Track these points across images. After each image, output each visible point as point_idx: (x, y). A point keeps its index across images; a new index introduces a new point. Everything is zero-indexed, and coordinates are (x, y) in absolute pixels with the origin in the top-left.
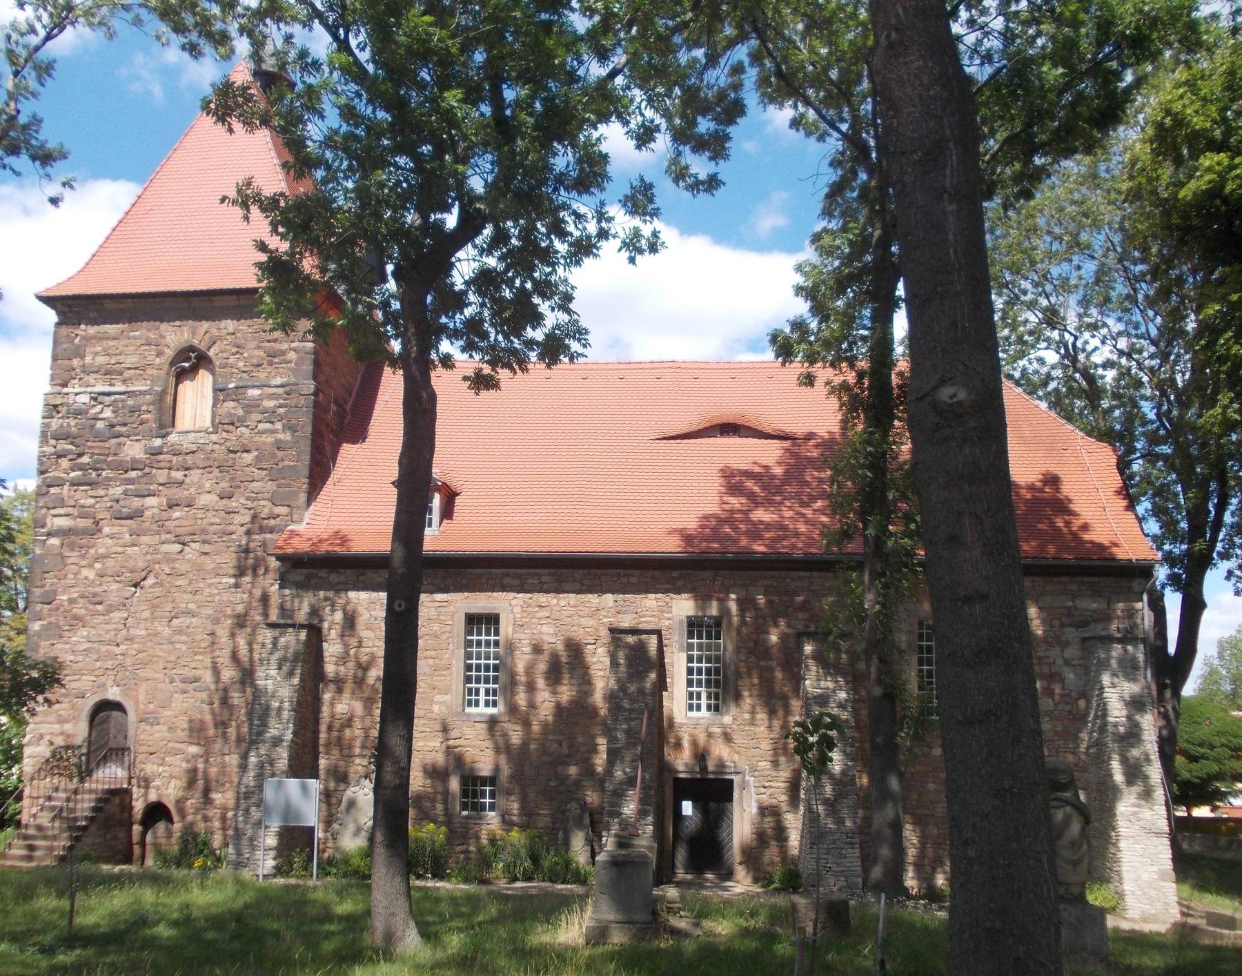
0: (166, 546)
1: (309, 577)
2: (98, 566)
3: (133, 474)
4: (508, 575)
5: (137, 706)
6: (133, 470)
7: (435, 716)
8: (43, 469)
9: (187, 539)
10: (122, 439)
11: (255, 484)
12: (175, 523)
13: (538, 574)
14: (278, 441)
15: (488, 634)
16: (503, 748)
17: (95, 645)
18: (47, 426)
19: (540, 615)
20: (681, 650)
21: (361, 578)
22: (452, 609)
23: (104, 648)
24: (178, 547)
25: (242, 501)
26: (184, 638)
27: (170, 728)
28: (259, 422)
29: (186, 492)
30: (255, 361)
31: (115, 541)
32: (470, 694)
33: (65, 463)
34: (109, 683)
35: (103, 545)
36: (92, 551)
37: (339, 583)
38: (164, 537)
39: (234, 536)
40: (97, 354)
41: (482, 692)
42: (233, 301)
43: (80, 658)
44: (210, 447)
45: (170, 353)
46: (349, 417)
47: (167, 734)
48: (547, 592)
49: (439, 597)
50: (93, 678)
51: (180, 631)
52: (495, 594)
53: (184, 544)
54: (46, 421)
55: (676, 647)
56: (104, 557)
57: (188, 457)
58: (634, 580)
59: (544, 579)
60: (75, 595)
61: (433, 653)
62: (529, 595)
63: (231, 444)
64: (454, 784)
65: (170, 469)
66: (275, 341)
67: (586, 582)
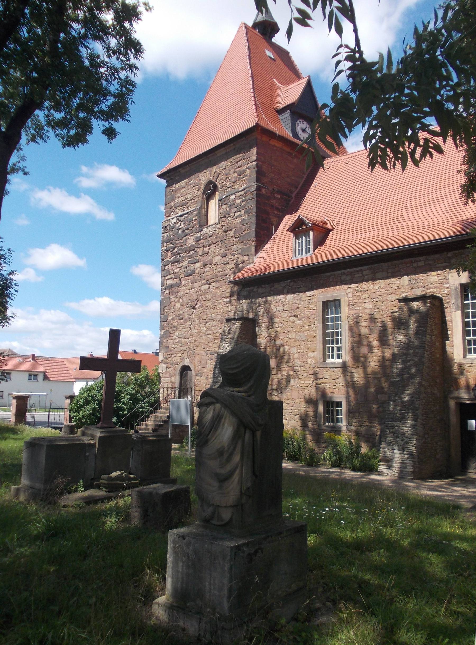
0: (203, 286)
1: (250, 292)
2: (181, 301)
3: (191, 253)
4: (344, 273)
5: (195, 368)
6: (191, 251)
7: (308, 365)
8: (163, 258)
9: (210, 281)
10: (187, 236)
11: (235, 247)
12: (206, 274)
13: (361, 270)
14: (243, 220)
15: (332, 314)
16: (350, 384)
17: (181, 339)
18: (163, 237)
19: (363, 297)
20: (457, 310)
21: (272, 289)
22: (315, 300)
23: (183, 340)
24: (208, 286)
25: (230, 257)
26: (210, 332)
27: (206, 378)
28: (235, 212)
29: (210, 257)
30: (233, 180)
31: (186, 287)
32: (469, 344)
33: (169, 253)
34: (186, 357)
35: (183, 290)
36: (179, 294)
37: (263, 293)
38: (203, 282)
39: (227, 277)
40: (179, 197)
41: (335, 349)
42: (223, 151)
43: (176, 346)
44: (217, 232)
45: (202, 187)
46: (293, 200)
47: (206, 381)
48: (367, 281)
49: (309, 293)
50: (180, 355)
51: (209, 329)
52: (337, 287)
53: (210, 284)
54: (163, 235)
55: (453, 307)
56: (183, 296)
57: (210, 239)
58: (421, 264)
59: (365, 273)
60: (174, 316)
61: (307, 328)
62: (356, 285)
63: (225, 228)
64: (321, 408)
65: (204, 247)
66: (241, 166)
67: (390, 271)
